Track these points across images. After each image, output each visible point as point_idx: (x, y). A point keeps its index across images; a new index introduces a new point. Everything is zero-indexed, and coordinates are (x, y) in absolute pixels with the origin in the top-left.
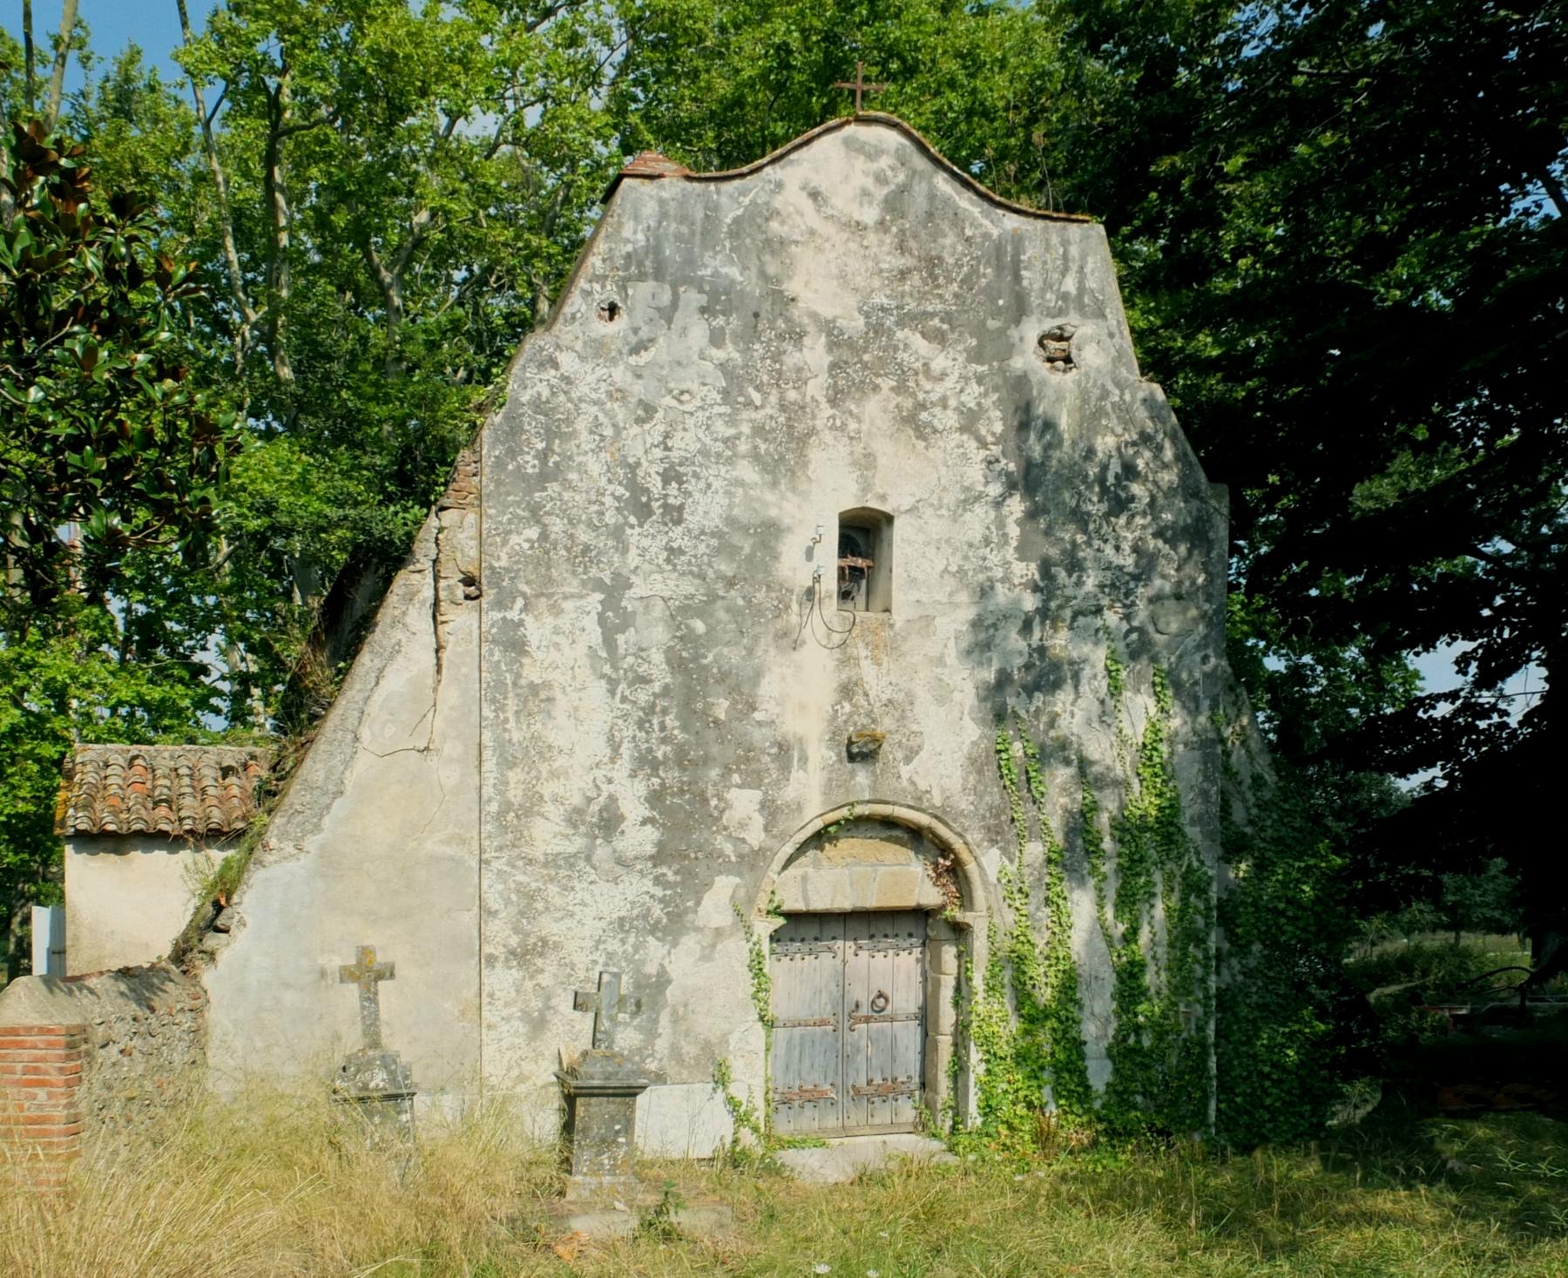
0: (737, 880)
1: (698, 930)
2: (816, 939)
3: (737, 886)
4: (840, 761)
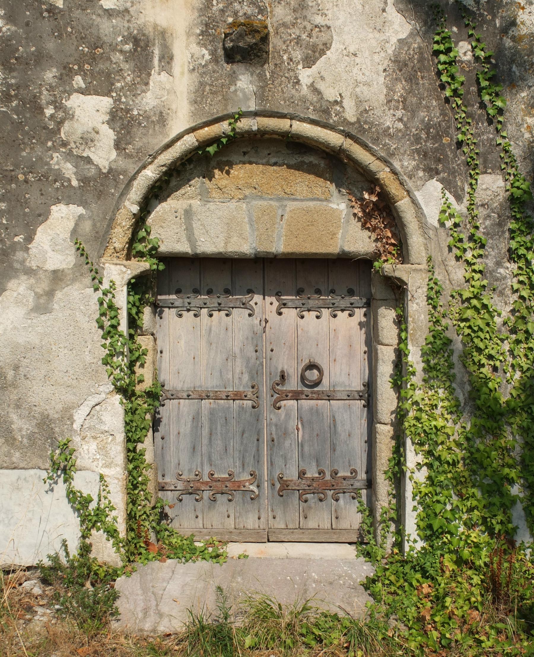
0: (81, 210)
1: (30, 272)
2: (227, 292)
3: (81, 217)
4: (215, 60)
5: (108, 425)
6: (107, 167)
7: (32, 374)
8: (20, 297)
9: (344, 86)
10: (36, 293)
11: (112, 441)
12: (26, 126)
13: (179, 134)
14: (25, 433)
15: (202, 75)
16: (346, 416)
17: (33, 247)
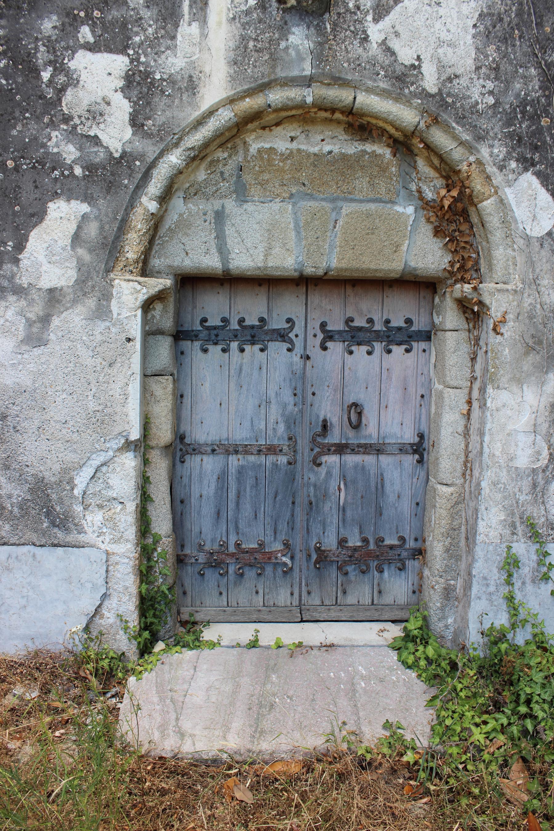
0: (85, 208)
3: (84, 217)
5: (117, 491)
6: (120, 151)
7: (23, 425)
8: (8, 323)
9: (424, 45)
10: (28, 320)
11: (121, 510)
12: (17, 94)
13: (212, 106)
14: (15, 501)
15: (244, 26)
16: (396, 474)
17: (25, 257)
